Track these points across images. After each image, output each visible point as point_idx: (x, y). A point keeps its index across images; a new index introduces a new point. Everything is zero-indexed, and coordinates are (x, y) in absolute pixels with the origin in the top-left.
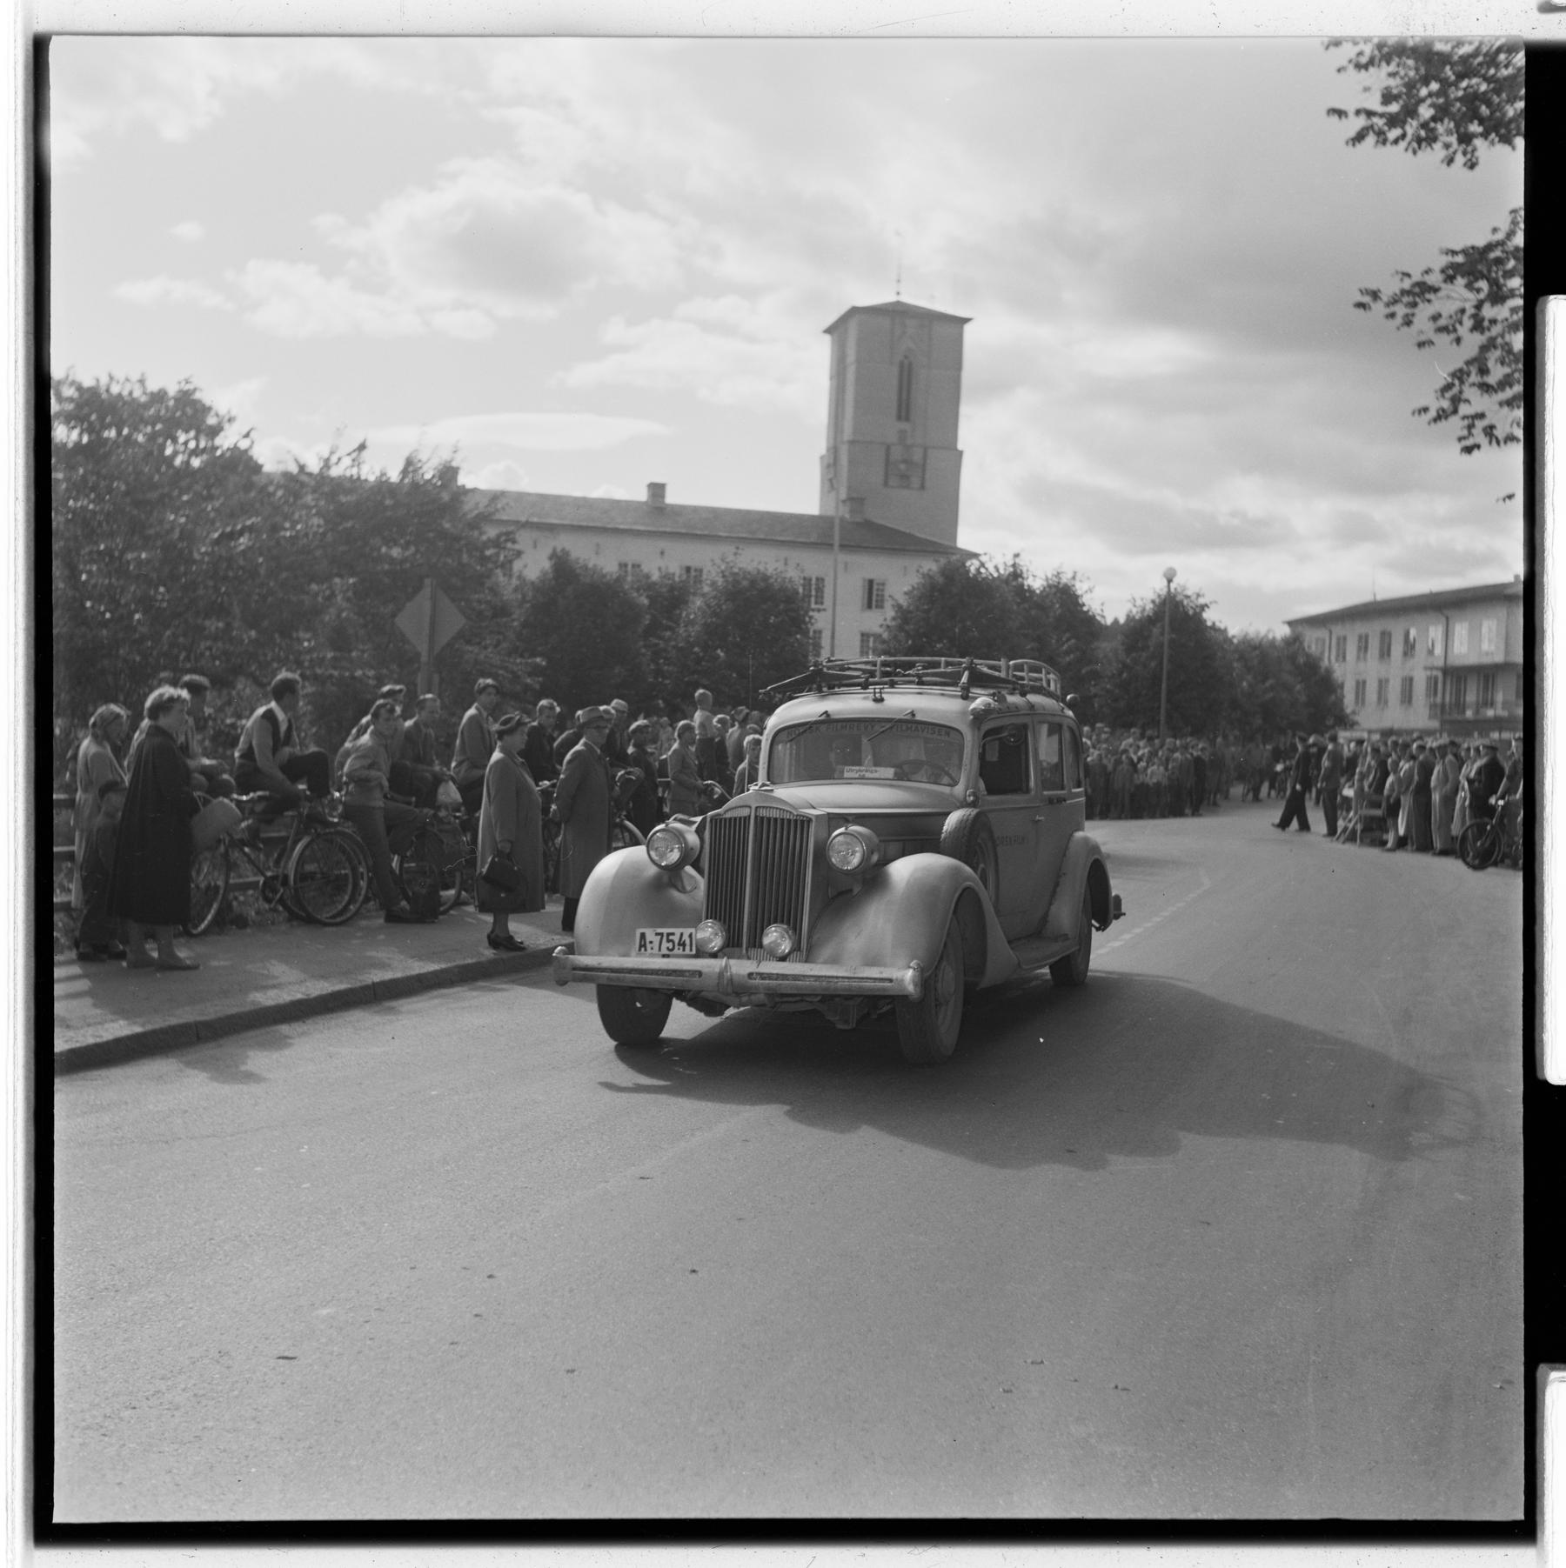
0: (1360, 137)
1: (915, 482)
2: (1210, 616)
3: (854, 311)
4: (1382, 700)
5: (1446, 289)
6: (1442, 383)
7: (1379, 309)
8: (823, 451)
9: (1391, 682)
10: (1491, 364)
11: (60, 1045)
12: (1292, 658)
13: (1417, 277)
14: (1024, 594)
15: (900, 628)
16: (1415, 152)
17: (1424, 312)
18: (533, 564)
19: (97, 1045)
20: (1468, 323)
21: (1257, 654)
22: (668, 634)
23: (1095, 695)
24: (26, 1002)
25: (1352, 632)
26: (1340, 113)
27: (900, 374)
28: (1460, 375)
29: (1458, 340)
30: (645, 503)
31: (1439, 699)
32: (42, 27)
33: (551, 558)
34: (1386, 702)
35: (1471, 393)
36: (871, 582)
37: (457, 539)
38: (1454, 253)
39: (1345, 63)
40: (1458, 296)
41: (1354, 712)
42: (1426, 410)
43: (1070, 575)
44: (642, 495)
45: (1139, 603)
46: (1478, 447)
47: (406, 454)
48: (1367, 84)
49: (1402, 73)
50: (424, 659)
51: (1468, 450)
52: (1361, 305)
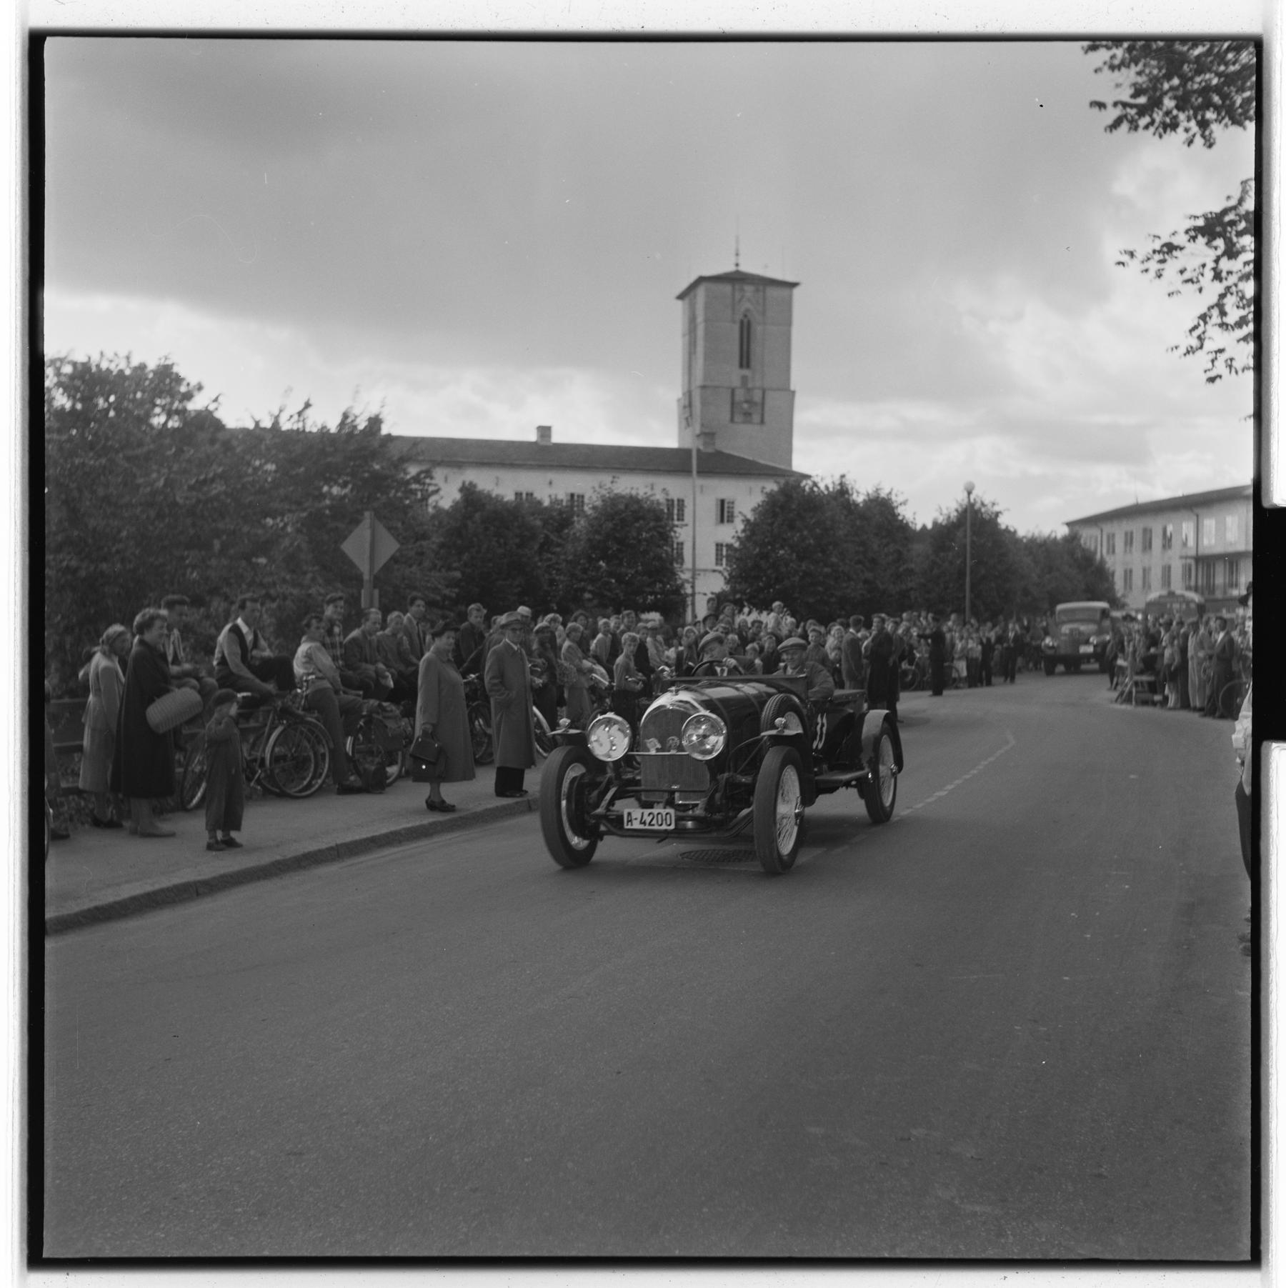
0: (1116, 124)
1: (756, 418)
2: (1003, 521)
3: (701, 280)
5: (1190, 247)
6: (1191, 325)
7: (1135, 265)
9: (1153, 572)
10: (1228, 308)
11: (50, 914)
12: (1072, 554)
13: (1166, 239)
15: (748, 538)
16: (1161, 136)
17: (1172, 266)
18: (446, 492)
19: (116, 903)
20: (1209, 274)
21: (1042, 549)
22: (558, 549)
26: (1101, 105)
28: (1204, 317)
29: (1200, 290)
30: (535, 443)
31: (1193, 583)
33: (461, 490)
36: (722, 502)
37: (386, 478)
38: (1196, 217)
39: (1100, 64)
40: (1201, 253)
41: (1124, 596)
44: (532, 437)
48: (1120, 80)
49: (1147, 71)
50: (366, 577)
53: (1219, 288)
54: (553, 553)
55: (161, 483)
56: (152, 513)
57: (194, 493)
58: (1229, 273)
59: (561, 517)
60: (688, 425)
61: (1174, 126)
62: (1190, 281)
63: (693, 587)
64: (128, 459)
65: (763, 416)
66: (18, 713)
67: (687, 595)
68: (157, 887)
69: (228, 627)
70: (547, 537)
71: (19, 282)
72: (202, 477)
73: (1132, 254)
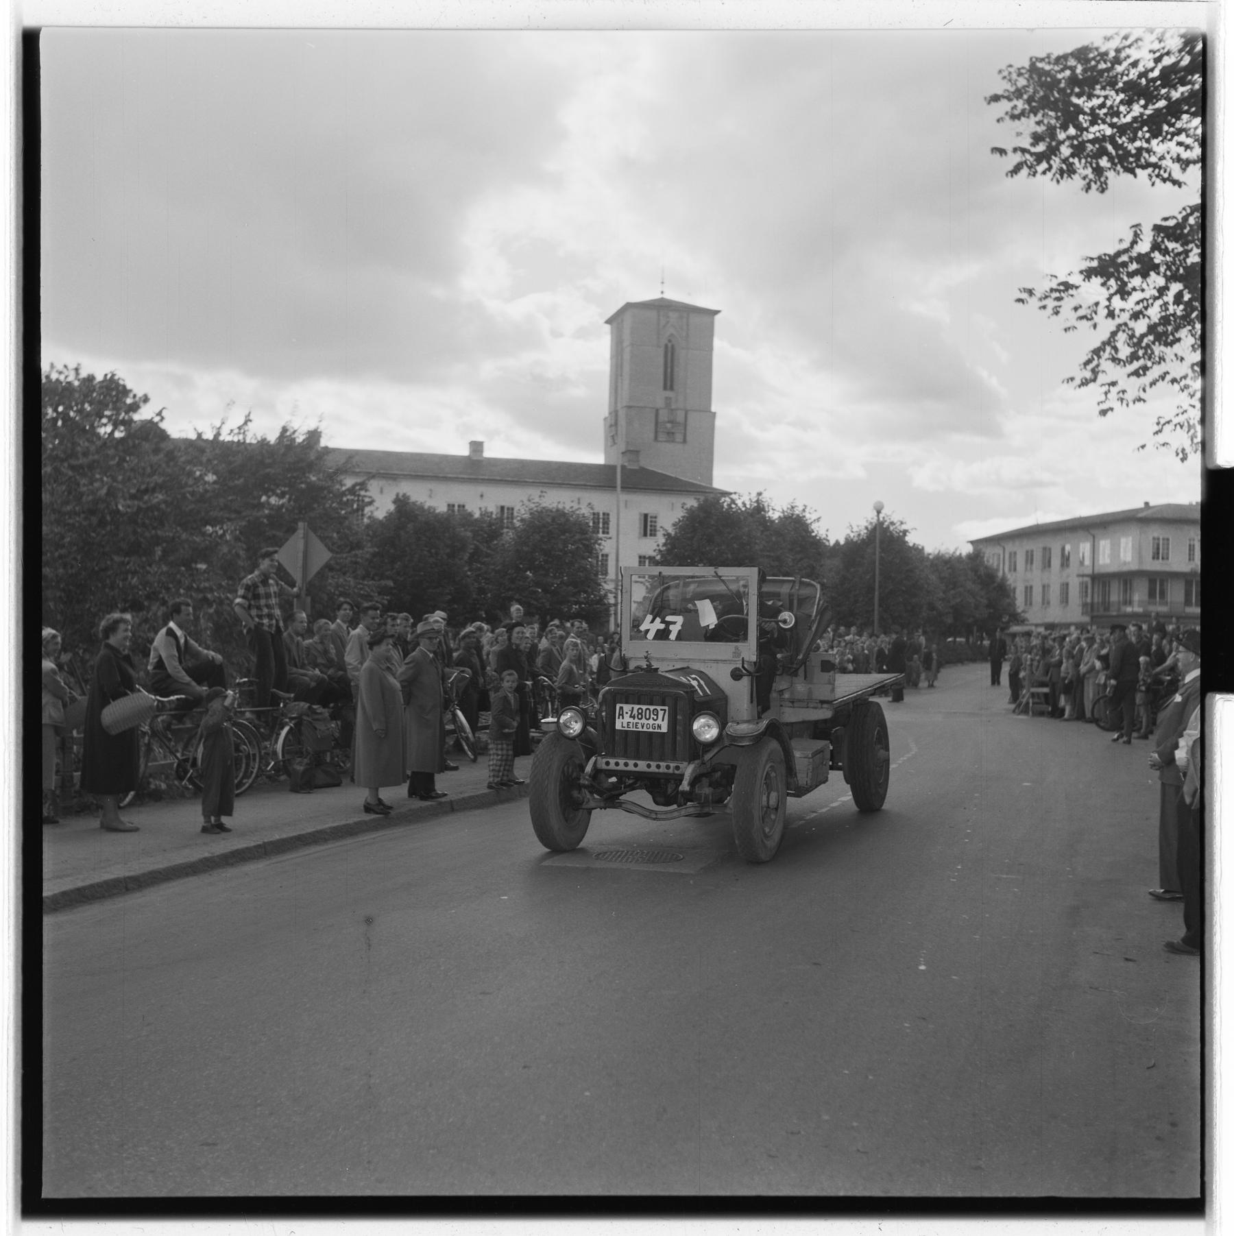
0: (1016, 170)
1: (679, 437)
2: (911, 539)
3: (629, 306)
4: (1046, 602)
6: (1085, 358)
7: (1034, 302)
10: (1119, 345)
12: (975, 571)
13: (1062, 279)
14: (765, 524)
17: (1067, 304)
18: (381, 505)
20: (1103, 312)
21: (946, 565)
25: (1020, 549)
26: (1002, 152)
27: (664, 352)
28: (1097, 352)
29: (1095, 326)
30: (468, 458)
31: (1089, 600)
32: (30, 22)
33: (394, 502)
34: (1049, 603)
35: (1106, 365)
36: (646, 516)
38: (1092, 259)
39: (1002, 115)
40: (1094, 291)
42: (1072, 379)
43: (801, 508)
44: (464, 451)
46: (1112, 409)
47: (283, 424)
51: (1104, 413)
53: (1111, 325)
54: (483, 563)
55: (104, 491)
56: (94, 520)
57: (136, 502)
58: (1122, 310)
59: (489, 529)
60: (615, 443)
61: (1069, 171)
63: (616, 597)
64: (72, 468)
66: (13, 666)
67: (610, 605)
68: (88, 882)
69: (164, 630)
70: (477, 548)
71: (13, 252)
72: (143, 487)
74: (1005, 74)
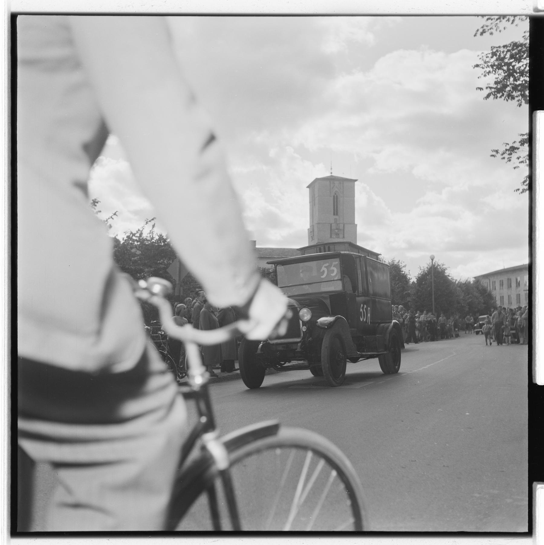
0: (488, 96)
2: (447, 273)
3: (317, 180)
5: (521, 148)
6: (523, 180)
7: (499, 156)
8: (309, 227)
12: (478, 288)
13: (511, 145)
17: (514, 156)
21: (466, 287)
23: (409, 301)
24: (8, 356)
25: (497, 280)
26: (481, 89)
34: (511, 303)
38: (523, 135)
39: (480, 75)
42: (519, 190)
43: (397, 261)
45: (422, 268)
48: (488, 82)
50: (177, 282)
52: (492, 156)
62: (522, 162)
65: (344, 235)
73: (497, 152)
74: (481, 57)
